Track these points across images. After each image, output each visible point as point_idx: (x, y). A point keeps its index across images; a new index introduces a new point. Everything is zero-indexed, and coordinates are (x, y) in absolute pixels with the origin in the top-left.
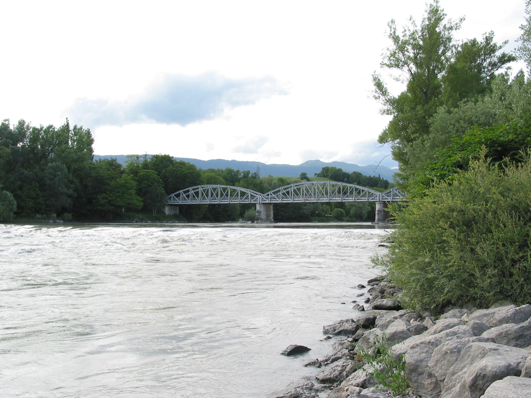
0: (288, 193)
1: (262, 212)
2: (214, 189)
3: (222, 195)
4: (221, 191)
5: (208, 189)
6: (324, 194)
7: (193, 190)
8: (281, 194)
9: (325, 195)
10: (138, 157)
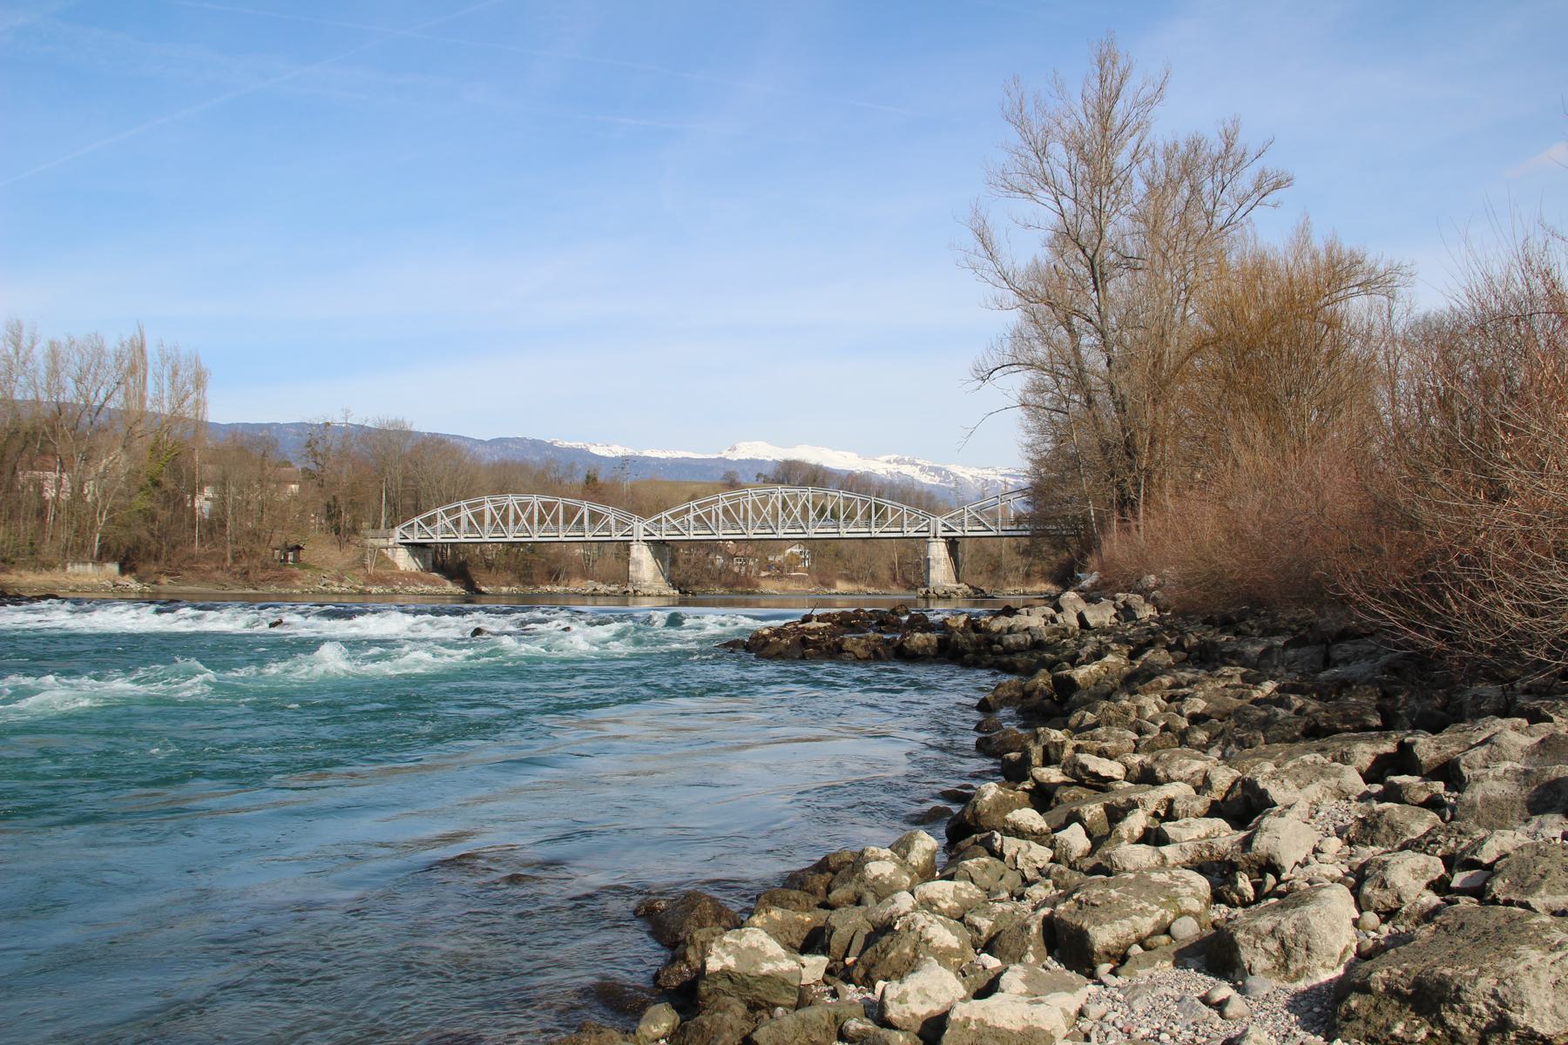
0: (709, 515)
1: (644, 564)
2: (524, 506)
3: (542, 521)
4: (540, 511)
5: (508, 505)
6: (769, 519)
7: (470, 506)
8: (691, 519)
9: (800, 520)
10: (763, 462)
